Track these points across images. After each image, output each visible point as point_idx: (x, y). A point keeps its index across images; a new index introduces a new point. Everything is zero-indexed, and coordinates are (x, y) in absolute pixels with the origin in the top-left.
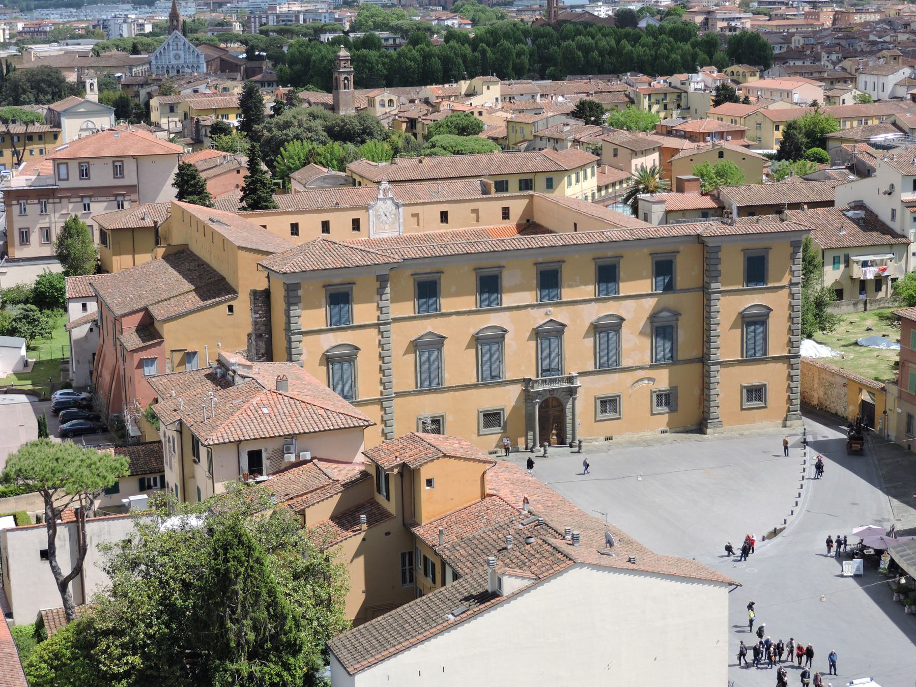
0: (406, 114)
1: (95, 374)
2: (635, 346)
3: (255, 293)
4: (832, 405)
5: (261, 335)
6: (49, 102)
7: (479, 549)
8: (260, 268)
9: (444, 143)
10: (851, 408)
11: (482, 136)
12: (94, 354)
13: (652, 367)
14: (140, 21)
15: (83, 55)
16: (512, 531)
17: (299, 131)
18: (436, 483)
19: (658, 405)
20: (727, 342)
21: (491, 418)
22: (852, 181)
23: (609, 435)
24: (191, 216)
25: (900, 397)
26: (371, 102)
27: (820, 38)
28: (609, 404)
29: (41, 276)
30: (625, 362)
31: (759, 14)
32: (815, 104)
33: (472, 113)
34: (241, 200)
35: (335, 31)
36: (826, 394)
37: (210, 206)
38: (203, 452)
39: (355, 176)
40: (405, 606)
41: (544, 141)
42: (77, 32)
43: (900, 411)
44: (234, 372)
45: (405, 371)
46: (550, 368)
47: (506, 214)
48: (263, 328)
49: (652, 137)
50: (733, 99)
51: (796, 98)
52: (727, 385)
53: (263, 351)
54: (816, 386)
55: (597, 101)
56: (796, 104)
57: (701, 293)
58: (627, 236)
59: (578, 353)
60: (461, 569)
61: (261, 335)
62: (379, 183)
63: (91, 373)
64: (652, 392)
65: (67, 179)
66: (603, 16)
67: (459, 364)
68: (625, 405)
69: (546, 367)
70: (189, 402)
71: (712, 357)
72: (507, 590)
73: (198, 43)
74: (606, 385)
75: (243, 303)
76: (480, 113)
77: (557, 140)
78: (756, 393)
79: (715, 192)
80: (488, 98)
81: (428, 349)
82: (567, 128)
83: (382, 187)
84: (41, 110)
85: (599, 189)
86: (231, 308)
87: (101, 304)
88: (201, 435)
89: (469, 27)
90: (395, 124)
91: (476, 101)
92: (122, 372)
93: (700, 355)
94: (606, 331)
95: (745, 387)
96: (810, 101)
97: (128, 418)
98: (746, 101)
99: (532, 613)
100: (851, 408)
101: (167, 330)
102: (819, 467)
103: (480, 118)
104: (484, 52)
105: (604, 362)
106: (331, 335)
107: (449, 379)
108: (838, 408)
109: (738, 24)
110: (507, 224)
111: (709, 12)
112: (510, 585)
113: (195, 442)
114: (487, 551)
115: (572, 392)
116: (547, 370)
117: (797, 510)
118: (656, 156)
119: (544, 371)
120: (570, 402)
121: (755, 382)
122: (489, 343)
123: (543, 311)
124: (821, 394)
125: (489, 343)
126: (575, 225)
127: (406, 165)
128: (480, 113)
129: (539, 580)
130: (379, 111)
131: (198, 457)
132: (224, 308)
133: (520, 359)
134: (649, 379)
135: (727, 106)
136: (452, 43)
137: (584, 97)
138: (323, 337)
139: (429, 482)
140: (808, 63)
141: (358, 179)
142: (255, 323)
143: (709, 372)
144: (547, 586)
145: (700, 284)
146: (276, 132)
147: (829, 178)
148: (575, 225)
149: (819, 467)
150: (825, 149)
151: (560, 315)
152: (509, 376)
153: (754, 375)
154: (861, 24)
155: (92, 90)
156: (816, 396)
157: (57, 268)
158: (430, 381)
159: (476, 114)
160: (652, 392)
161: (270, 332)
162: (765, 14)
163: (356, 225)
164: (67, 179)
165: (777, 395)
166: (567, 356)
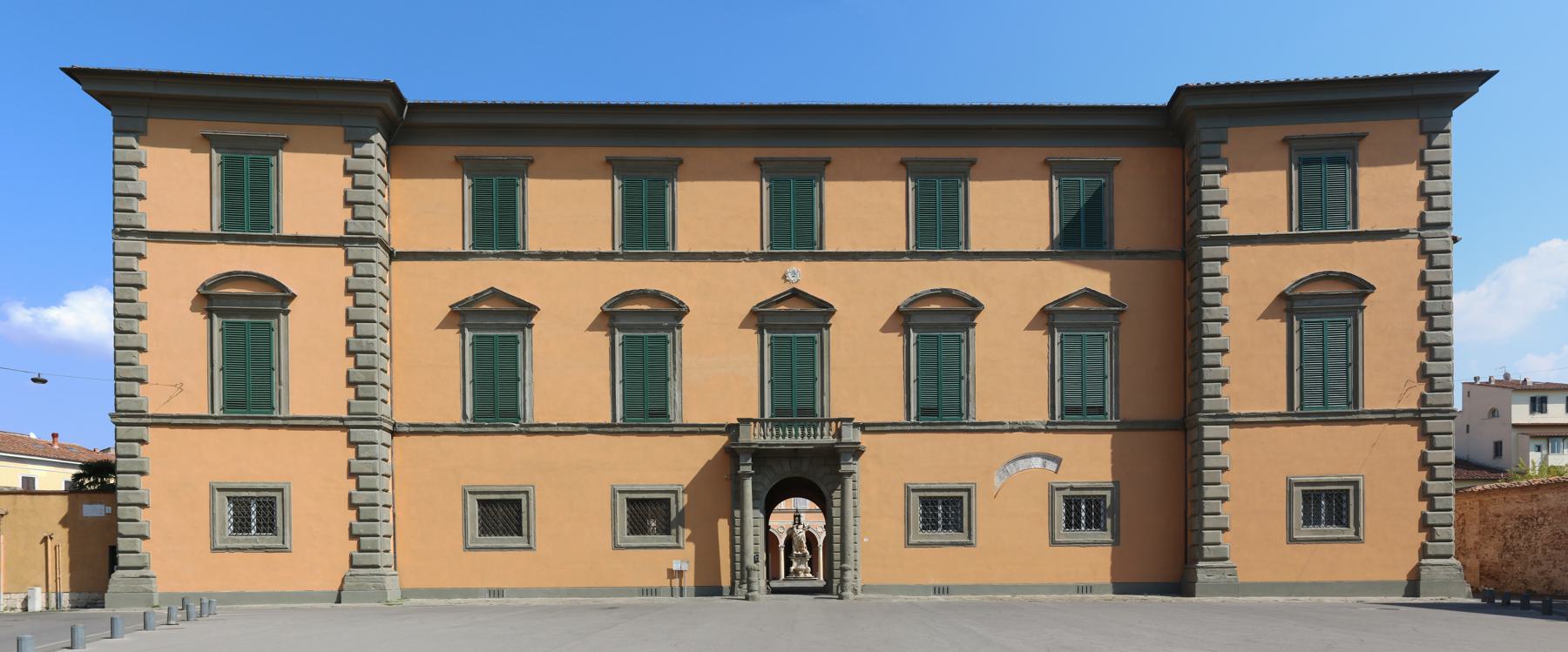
2: (1010, 365)
13: (1051, 428)
19: (1068, 525)
20: (1250, 359)
21: (647, 514)
28: (944, 512)
36: (1506, 548)
52: (1251, 476)
59: (864, 374)
64: (1053, 489)
67: (569, 368)
68: (983, 513)
74: (938, 459)
78: (1329, 505)
81: (495, 336)
94: (937, 335)
95: (1298, 484)
107: (540, 402)
108: (1555, 573)
120: (837, 494)
122: (644, 338)
123: (777, 267)
125: (644, 338)
133: (720, 376)
134: (1047, 457)
152: (692, 416)
153: (1325, 452)
158: (496, 400)
160: (1053, 489)
165: (1390, 533)
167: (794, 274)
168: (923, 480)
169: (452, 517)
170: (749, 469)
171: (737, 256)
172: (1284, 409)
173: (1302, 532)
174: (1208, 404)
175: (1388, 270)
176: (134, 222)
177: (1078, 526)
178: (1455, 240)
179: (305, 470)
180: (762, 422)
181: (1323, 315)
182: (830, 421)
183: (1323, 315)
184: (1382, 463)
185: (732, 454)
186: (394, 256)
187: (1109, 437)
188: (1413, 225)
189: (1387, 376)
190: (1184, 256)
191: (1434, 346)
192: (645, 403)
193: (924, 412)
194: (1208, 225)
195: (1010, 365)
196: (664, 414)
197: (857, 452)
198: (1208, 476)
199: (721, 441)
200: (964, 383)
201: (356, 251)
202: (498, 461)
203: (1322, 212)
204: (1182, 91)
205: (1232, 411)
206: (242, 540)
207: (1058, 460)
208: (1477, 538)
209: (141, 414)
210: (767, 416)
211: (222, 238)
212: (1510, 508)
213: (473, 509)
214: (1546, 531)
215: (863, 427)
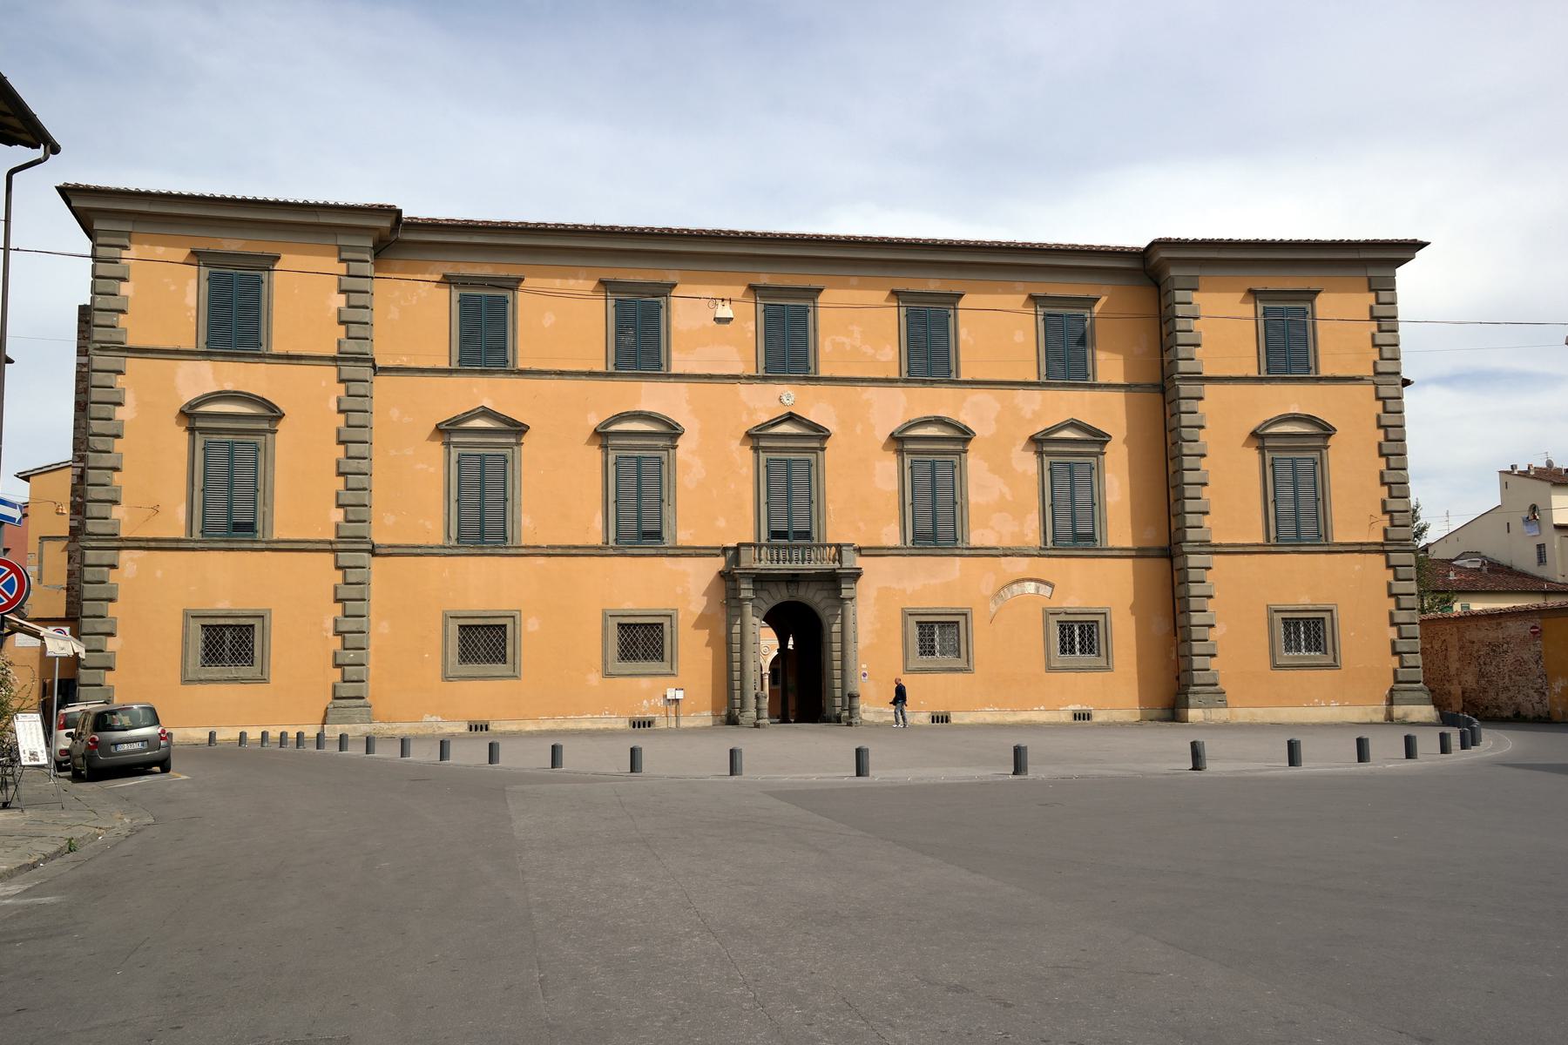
2: (1001, 493)
4: (1503, 697)
13: (1042, 553)
19: (1063, 651)
20: (1230, 492)
23: (941, 710)
28: (938, 635)
36: (1482, 675)
46: (790, 526)
52: (1239, 598)
54: (1454, 666)
57: (1159, 396)
59: (860, 499)
67: (560, 487)
68: (981, 638)
69: (781, 526)
74: (934, 582)
78: (1306, 633)
93: (1165, 544)
102: (1541, 558)
105: (926, 526)
106: (205, 367)
107: (530, 525)
108: (1520, 698)
119: (775, 534)
122: (638, 467)
124: (1470, 680)
133: (716, 498)
138: (185, 368)
143: (1184, 569)
145: (1158, 380)
149: (1541, 558)
151: (815, 404)
152: (684, 537)
153: (1302, 580)
158: (482, 523)
166: (830, 507)
167: (789, 397)
168: (912, 605)
169: (433, 645)
170: (750, 594)
171: (735, 378)
172: (1261, 540)
173: (1285, 657)
174: (1191, 534)
175: (1347, 412)
176: (367, 350)
177: (1072, 651)
178: (1406, 383)
179: (280, 589)
180: (757, 546)
181: (1294, 454)
182: (824, 546)
183: (1294, 454)
184: (1357, 595)
185: (728, 578)
186: (378, 370)
187: (1130, 561)
188: (1368, 371)
189: (1353, 509)
190: (1163, 392)
191: (1394, 483)
192: (640, 529)
193: (917, 537)
194: (1183, 366)
195: (1001, 493)
196: (657, 535)
197: (856, 575)
198: (1194, 604)
199: (719, 563)
200: (958, 507)
201: (349, 371)
202: (482, 584)
203: (1287, 352)
204: (1158, 244)
205: (1214, 541)
206: (215, 671)
207: (1052, 586)
208: (1457, 665)
209: (1206, 543)
210: (763, 541)
211: (765, 379)
212: (1481, 634)
213: (614, 633)
214: (1510, 658)
215: (859, 550)
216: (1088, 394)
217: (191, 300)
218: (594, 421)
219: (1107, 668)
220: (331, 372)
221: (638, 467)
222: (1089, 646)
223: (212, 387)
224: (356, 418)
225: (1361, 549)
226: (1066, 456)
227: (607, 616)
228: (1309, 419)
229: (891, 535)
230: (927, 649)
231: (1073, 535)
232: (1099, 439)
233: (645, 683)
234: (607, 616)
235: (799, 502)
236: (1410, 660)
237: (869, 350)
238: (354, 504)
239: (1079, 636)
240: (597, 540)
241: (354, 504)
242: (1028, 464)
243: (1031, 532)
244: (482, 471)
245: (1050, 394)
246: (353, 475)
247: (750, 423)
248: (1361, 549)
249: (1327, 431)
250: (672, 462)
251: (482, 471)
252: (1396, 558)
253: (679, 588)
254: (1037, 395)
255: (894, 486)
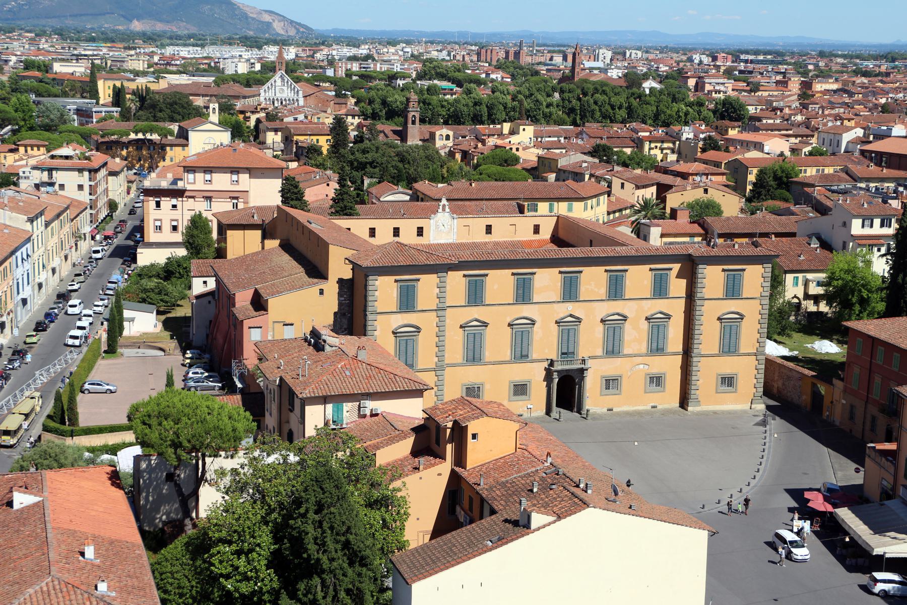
0: (459, 147)
1: (210, 336)
2: (635, 336)
3: (341, 282)
5: (344, 314)
6: (179, 121)
7: (514, 491)
8: (347, 262)
9: (489, 171)
10: (804, 397)
11: (519, 167)
12: (211, 321)
14: (252, 61)
15: (207, 86)
16: (537, 479)
17: (376, 155)
18: (479, 437)
20: (708, 335)
22: (812, 218)
23: (610, 407)
24: (293, 218)
25: (845, 390)
26: (432, 136)
27: (789, 101)
28: (611, 383)
29: (168, 259)
30: (626, 351)
31: (739, 80)
32: (782, 154)
33: (511, 149)
34: (332, 207)
35: (404, 78)
36: (783, 384)
37: (309, 211)
38: (297, 403)
39: (419, 194)
40: (453, 533)
41: (567, 174)
42: (202, 66)
43: (844, 402)
44: (325, 341)
45: (456, 342)
47: (537, 230)
48: (347, 308)
49: (652, 174)
50: (716, 148)
51: (766, 149)
52: (707, 371)
53: (345, 326)
54: (776, 378)
55: (608, 144)
56: (768, 154)
58: (633, 253)
59: (591, 340)
60: (496, 506)
61: (344, 314)
62: (440, 200)
63: (207, 335)
65: (194, 183)
66: (615, 77)
67: (498, 342)
68: (625, 384)
69: (565, 351)
70: (287, 363)
71: (695, 351)
72: (534, 525)
73: (297, 80)
75: (331, 287)
76: (517, 149)
77: (576, 174)
78: (728, 381)
79: (701, 221)
80: (524, 142)
82: (584, 165)
83: (441, 204)
84: (175, 127)
85: (609, 213)
86: (321, 292)
87: (218, 282)
88: (297, 390)
89: (509, 80)
90: (451, 154)
91: (514, 139)
92: (233, 337)
96: (778, 152)
97: (236, 372)
98: (727, 150)
99: (551, 542)
100: (804, 397)
101: (273, 303)
103: (518, 153)
104: (520, 102)
105: (610, 349)
107: (488, 355)
109: (722, 88)
110: (179, 204)
111: (699, 78)
112: (537, 519)
113: (292, 394)
114: (516, 493)
115: (582, 371)
116: (567, 354)
117: (758, 475)
118: (654, 189)
119: (563, 354)
121: (727, 371)
122: (522, 333)
124: (780, 384)
126: (591, 241)
127: (460, 186)
128: (517, 149)
129: (559, 518)
130: (439, 143)
131: (293, 407)
132: (316, 289)
133: (545, 344)
135: (711, 155)
136: (497, 94)
137: (598, 141)
138: (394, 316)
139: (474, 436)
140: (778, 121)
141: (421, 196)
142: (340, 304)
144: (563, 521)
146: (359, 155)
147: (793, 214)
148: (591, 241)
150: (788, 191)
153: (728, 365)
154: (821, 92)
155: (214, 113)
156: (776, 386)
157: (182, 252)
158: (474, 356)
159: (514, 150)
161: (352, 312)
162: (744, 81)
163: (420, 232)
164: (194, 183)
195: (635, 336)
198: (694, 373)
199: (546, 364)
213: (512, 387)
216: (666, 300)
217: (395, 295)
218: (509, 320)
219: (664, 391)
220: (434, 313)
221: (522, 333)
222: (658, 384)
223: (401, 323)
224: (442, 329)
225: (749, 354)
226: (657, 323)
227: (510, 382)
228: (737, 313)
229: (599, 352)
230: (608, 388)
231: (657, 348)
232: (668, 317)
233: (520, 403)
234: (510, 382)
235: (571, 342)
236: (765, 307)
237: (596, 290)
238: (440, 356)
239: (657, 380)
240: (508, 358)
241: (440, 356)
242: (645, 325)
243: (643, 348)
244: (474, 335)
245: (399, 315)
246: (440, 346)
247: (558, 318)
248: (749, 354)
249: (742, 317)
250: (532, 331)
251: (474, 335)
252: (759, 357)
253: (534, 374)
254: (649, 302)
255: (601, 336)
